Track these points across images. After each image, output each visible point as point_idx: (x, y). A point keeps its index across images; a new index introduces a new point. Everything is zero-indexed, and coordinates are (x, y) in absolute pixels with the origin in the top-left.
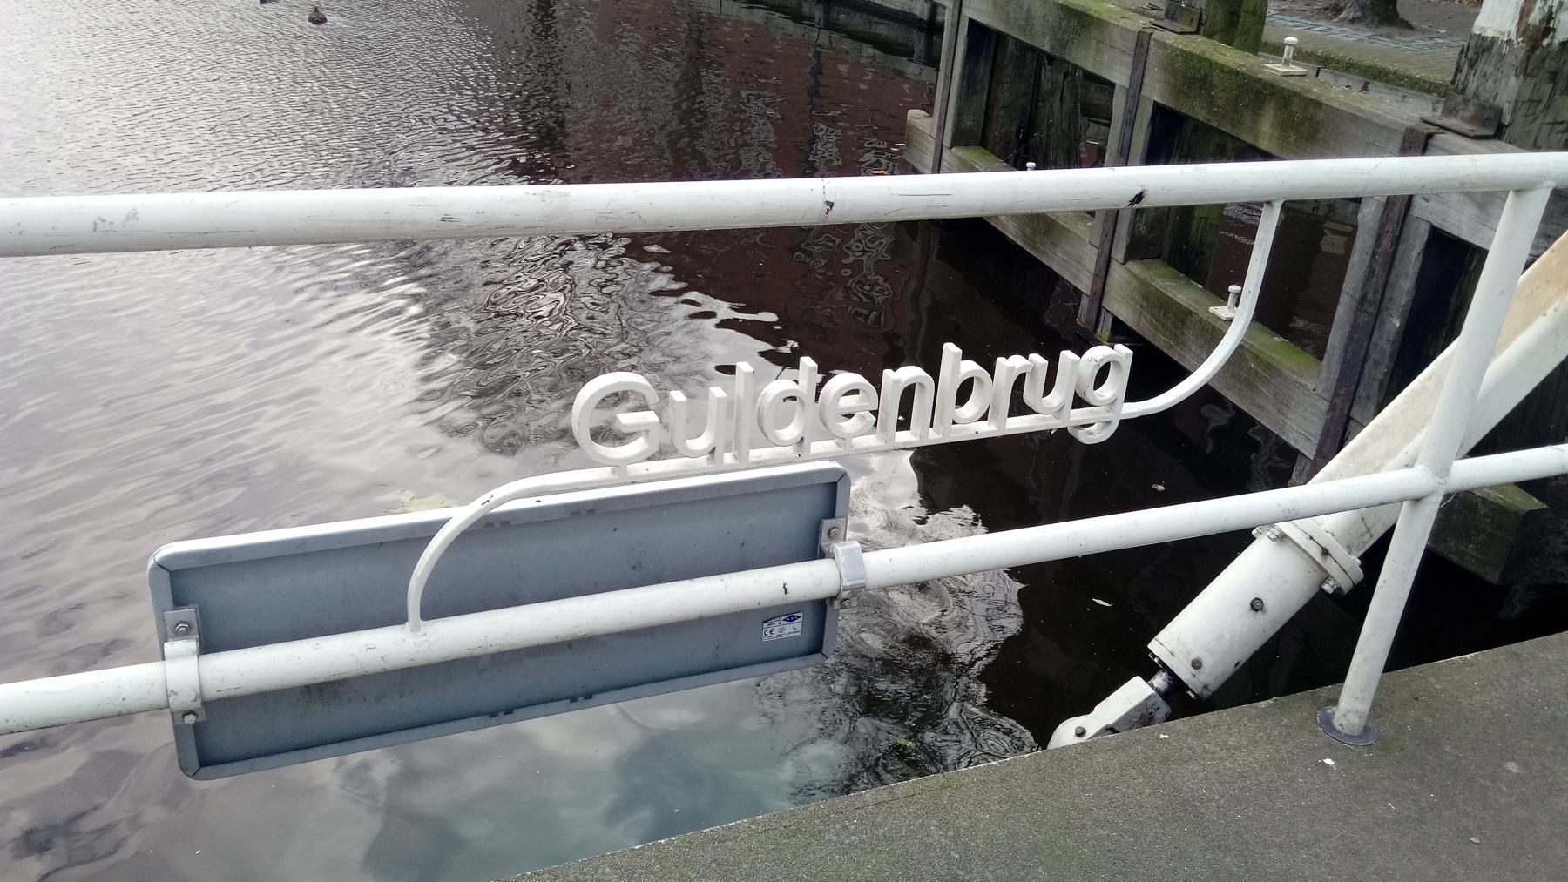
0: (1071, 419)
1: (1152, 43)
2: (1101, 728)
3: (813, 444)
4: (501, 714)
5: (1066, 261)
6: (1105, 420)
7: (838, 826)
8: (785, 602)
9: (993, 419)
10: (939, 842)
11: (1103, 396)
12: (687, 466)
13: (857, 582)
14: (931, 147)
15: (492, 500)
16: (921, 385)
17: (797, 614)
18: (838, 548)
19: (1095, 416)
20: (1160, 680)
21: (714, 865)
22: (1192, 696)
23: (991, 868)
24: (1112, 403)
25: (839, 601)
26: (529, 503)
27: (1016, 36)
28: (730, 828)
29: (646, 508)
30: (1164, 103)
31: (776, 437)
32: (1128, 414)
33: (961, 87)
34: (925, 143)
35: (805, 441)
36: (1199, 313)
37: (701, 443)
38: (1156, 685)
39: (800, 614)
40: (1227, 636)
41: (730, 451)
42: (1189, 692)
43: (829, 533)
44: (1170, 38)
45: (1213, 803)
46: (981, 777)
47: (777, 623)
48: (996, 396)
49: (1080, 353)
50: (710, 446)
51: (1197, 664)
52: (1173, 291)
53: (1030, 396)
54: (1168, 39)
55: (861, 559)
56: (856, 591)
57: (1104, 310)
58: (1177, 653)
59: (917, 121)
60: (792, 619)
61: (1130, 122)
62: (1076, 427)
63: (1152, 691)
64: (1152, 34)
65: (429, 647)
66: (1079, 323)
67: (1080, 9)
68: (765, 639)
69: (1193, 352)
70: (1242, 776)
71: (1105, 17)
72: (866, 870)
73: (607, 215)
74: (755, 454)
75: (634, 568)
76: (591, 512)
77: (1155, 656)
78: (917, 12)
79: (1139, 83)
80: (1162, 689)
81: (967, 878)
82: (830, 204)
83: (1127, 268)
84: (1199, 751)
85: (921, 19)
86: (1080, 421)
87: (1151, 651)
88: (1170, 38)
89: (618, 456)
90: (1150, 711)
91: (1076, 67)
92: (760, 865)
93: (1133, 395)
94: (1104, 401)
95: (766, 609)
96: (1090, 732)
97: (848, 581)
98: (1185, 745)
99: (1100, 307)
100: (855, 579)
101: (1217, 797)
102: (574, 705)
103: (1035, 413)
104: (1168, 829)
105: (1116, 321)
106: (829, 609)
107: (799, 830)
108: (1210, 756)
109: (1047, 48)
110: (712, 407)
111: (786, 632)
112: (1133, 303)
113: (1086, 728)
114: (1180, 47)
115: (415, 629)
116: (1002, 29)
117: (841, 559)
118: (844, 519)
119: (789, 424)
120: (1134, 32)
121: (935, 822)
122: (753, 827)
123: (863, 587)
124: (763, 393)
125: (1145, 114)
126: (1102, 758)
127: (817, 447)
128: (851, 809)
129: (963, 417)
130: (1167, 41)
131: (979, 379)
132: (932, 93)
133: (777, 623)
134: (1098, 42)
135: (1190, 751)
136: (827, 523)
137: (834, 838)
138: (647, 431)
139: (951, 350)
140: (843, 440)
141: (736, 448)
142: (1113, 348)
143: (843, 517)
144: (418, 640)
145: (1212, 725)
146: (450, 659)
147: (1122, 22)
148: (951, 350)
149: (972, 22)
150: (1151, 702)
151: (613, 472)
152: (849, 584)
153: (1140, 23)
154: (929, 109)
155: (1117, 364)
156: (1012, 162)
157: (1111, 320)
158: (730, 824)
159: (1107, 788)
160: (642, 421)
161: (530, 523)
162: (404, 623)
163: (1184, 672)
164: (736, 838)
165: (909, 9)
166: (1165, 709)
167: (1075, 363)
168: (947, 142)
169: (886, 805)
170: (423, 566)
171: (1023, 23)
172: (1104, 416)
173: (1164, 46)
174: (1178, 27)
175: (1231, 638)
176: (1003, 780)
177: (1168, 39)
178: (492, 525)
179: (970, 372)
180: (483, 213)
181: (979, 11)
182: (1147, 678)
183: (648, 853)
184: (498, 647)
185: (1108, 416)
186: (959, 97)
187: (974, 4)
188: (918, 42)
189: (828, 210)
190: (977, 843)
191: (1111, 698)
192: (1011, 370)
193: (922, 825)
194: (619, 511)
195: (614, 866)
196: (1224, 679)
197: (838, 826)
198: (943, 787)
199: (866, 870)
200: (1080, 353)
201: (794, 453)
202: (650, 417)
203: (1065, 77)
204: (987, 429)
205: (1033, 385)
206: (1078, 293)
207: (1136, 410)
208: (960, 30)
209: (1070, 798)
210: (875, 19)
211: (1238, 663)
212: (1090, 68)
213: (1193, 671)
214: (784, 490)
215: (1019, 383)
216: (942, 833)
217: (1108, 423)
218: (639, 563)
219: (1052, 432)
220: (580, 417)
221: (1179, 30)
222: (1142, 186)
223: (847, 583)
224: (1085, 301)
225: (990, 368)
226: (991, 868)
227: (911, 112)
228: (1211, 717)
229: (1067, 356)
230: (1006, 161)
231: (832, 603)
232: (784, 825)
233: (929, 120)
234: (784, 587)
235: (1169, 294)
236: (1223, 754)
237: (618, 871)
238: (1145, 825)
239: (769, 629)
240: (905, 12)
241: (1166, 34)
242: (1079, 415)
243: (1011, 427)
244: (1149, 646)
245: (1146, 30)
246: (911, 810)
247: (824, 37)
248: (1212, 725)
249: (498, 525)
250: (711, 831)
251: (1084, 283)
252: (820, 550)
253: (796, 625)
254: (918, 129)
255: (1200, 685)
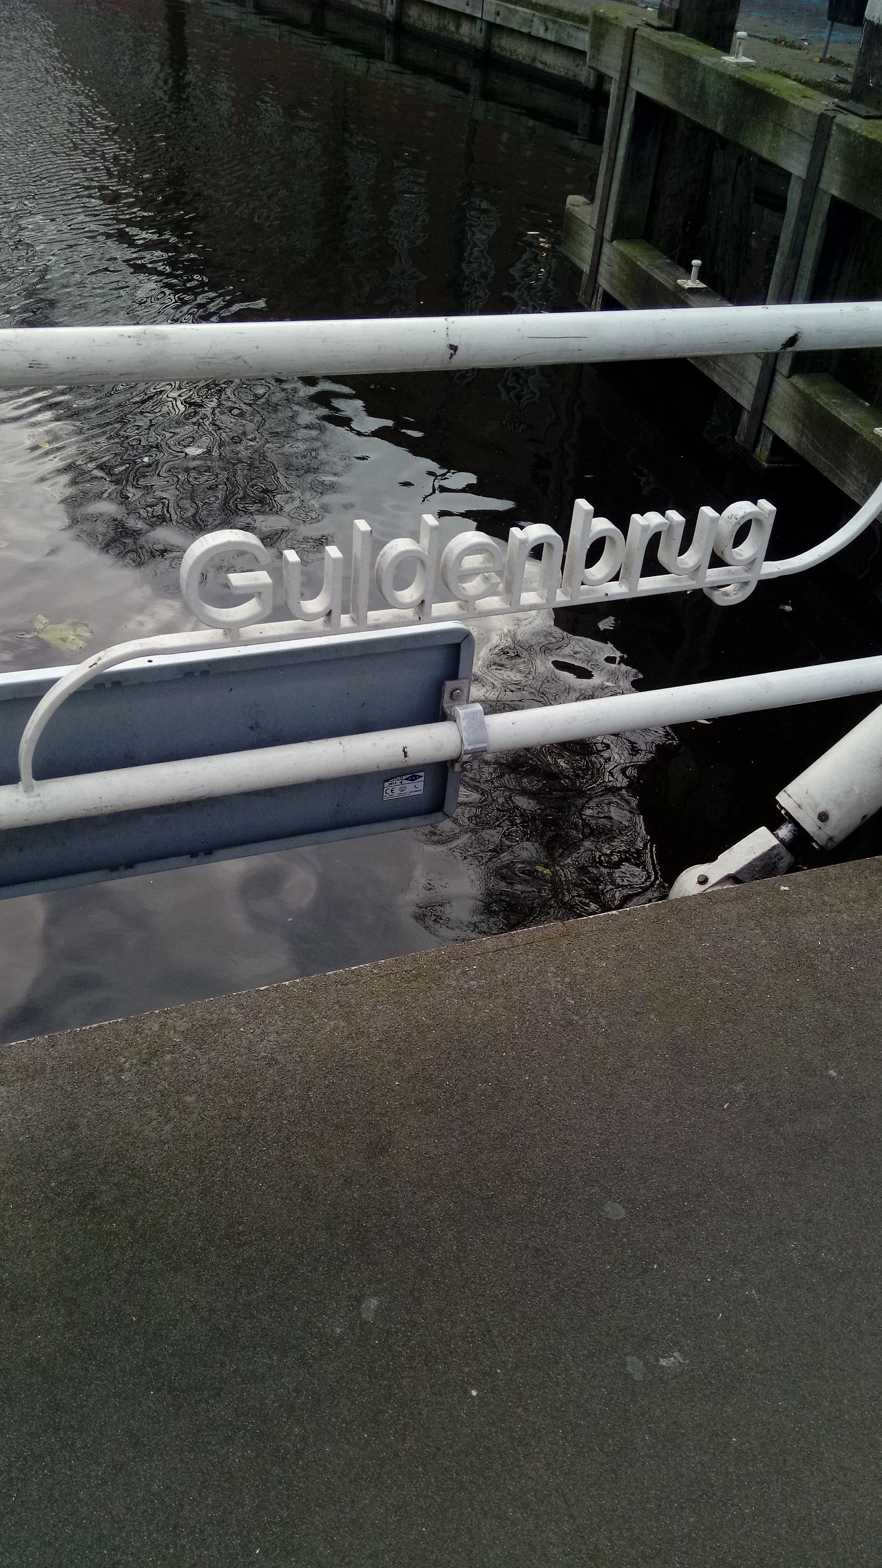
0: (707, 580)
1: (834, 128)
2: (723, 876)
3: (433, 605)
4: (122, 868)
5: (728, 373)
6: (743, 581)
7: (458, 971)
8: (405, 765)
9: (625, 580)
10: (556, 989)
11: (741, 556)
12: (301, 629)
13: (478, 746)
14: (590, 238)
15: (99, 663)
16: (550, 545)
17: (420, 774)
18: (460, 711)
19: (732, 577)
20: (785, 831)
21: (336, 1007)
22: (817, 847)
23: (605, 1013)
24: (751, 563)
25: (460, 764)
26: (141, 663)
27: (687, 115)
28: (353, 971)
29: (262, 669)
30: (843, 198)
31: (395, 600)
32: (767, 574)
33: (625, 170)
34: (584, 235)
35: (426, 603)
36: (865, 434)
37: (314, 605)
38: (780, 836)
39: (422, 774)
40: (857, 790)
41: (348, 613)
42: (814, 844)
43: (452, 694)
44: (854, 123)
45: (828, 955)
46: (600, 927)
47: (398, 782)
48: (629, 556)
49: (720, 511)
50: (325, 609)
51: (823, 817)
52: (838, 409)
53: (663, 556)
54: (852, 123)
55: (483, 723)
56: (477, 754)
57: (764, 429)
58: (804, 806)
59: (577, 209)
60: (413, 778)
61: (804, 218)
62: (711, 588)
63: (775, 842)
64: (834, 117)
65: (43, 808)
66: (737, 441)
67: (757, 86)
68: (386, 797)
69: (854, 476)
70: (859, 928)
71: (785, 95)
72: (483, 1014)
73: (208, 360)
74: (373, 616)
75: (252, 728)
76: (205, 673)
77: (782, 808)
78: (583, 80)
79: (818, 172)
80: (787, 840)
81: (581, 1022)
82: (454, 348)
83: (792, 383)
84: (818, 902)
85: (586, 88)
86: (715, 582)
87: (778, 802)
88: (854, 123)
89: (229, 619)
90: (773, 861)
91: (750, 153)
92: (381, 1007)
93: (775, 552)
94: (742, 561)
95: (385, 772)
96: (713, 880)
97: (469, 745)
98: (804, 897)
99: (761, 424)
100: (476, 743)
101: (832, 949)
102: (194, 860)
103: (670, 573)
104: (781, 979)
105: (777, 440)
106: (450, 770)
107: (420, 975)
108: (828, 909)
109: (719, 129)
110: (328, 568)
111: (407, 791)
112: (795, 421)
113: (708, 877)
114: (864, 133)
115: (28, 790)
116: (673, 105)
117: (463, 723)
118: (467, 680)
119: (407, 587)
120: (815, 114)
121: (552, 969)
122: (375, 971)
123: (484, 751)
124: (381, 553)
125: (823, 206)
126: (721, 908)
127: (438, 609)
128: (472, 955)
129: (592, 578)
130: (851, 127)
131: (612, 539)
132: (593, 179)
133: (398, 782)
134: (776, 124)
135: (809, 904)
136: (449, 685)
137: (454, 983)
138: (260, 594)
139: (582, 505)
140: (466, 603)
141: (353, 611)
142: (756, 504)
143: (466, 678)
144: (32, 800)
145: (833, 878)
146: (65, 819)
147: (802, 103)
148: (582, 505)
149: (639, 96)
150: (775, 852)
151: (225, 634)
152: (470, 748)
153: (822, 103)
154: (591, 197)
155: (759, 522)
156: (676, 258)
157: (771, 439)
158: (353, 968)
159: (724, 939)
160: (253, 582)
161: (142, 683)
162: (17, 783)
163: (810, 824)
164: (358, 981)
165: (574, 76)
166: (787, 859)
167: (714, 521)
168: (608, 233)
169: (506, 952)
170: (32, 728)
171: (695, 100)
172: (743, 576)
173: (846, 131)
174: (863, 109)
175: (860, 792)
176: (622, 930)
177: (852, 123)
178: (103, 685)
179: (601, 531)
180: (73, 358)
181: (647, 83)
182: (773, 829)
183: (273, 994)
184: (114, 809)
185: (747, 576)
186: (623, 183)
187: (644, 75)
188: (581, 113)
189: (452, 355)
190: (592, 990)
191: (735, 847)
192: (645, 528)
193: (540, 972)
194: (233, 672)
195: (240, 1006)
196: (851, 830)
197: (458, 971)
198: (563, 936)
199: (483, 1014)
200: (720, 511)
201: (414, 616)
202: (262, 577)
203: (739, 161)
204: (617, 590)
205: (669, 545)
206: (739, 408)
207: (776, 570)
208: (626, 105)
209: (686, 948)
210: (537, 86)
211: (865, 816)
212: (765, 153)
213: (819, 823)
214: (405, 650)
215: (654, 541)
216: (558, 979)
217: (746, 583)
218: (257, 723)
219: (688, 593)
220: (188, 577)
221: (864, 114)
222: (796, 327)
223: (468, 747)
224: (745, 417)
225: (623, 525)
226: (605, 1013)
227: (571, 199)
228: (833, 870)
229: (707, 511)
230: (671, 258)
231: (453, 766)
232: (405, 969)
233: (589, 208)
234: (404, 751)
235: (833, 413)
236: (842, 907)
237: (244, 1011)
238: (759, 975)
239: (391, 788)
240: (568, 79)
241: (851, 118)
242: (714, 575)
243: (643, 588)
244: (777, 798)
245: (829, 113)
246: (530, 957)
247: (480, 109)
248: (833, 878)
249: (108, 685)
250: (335, 974)
251: (745, 398)
252: (442, 711)
253: (418, 785)
254: (577, 218)
255: (825, 838)
